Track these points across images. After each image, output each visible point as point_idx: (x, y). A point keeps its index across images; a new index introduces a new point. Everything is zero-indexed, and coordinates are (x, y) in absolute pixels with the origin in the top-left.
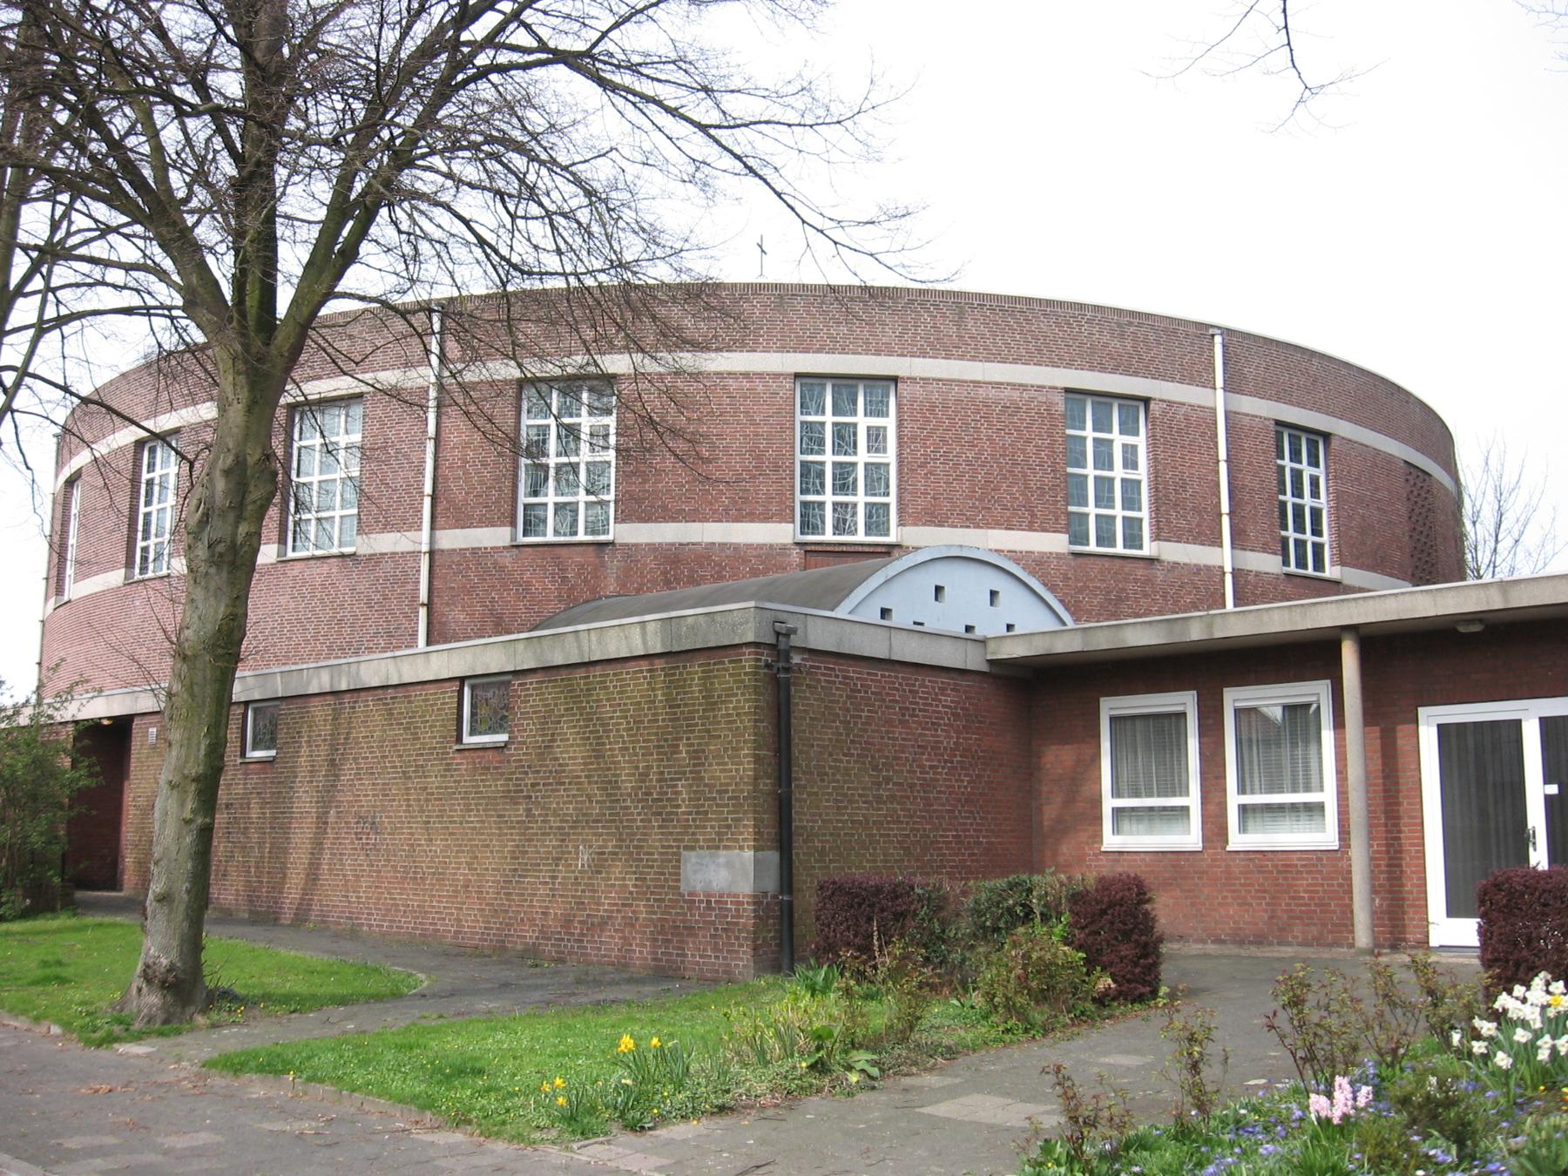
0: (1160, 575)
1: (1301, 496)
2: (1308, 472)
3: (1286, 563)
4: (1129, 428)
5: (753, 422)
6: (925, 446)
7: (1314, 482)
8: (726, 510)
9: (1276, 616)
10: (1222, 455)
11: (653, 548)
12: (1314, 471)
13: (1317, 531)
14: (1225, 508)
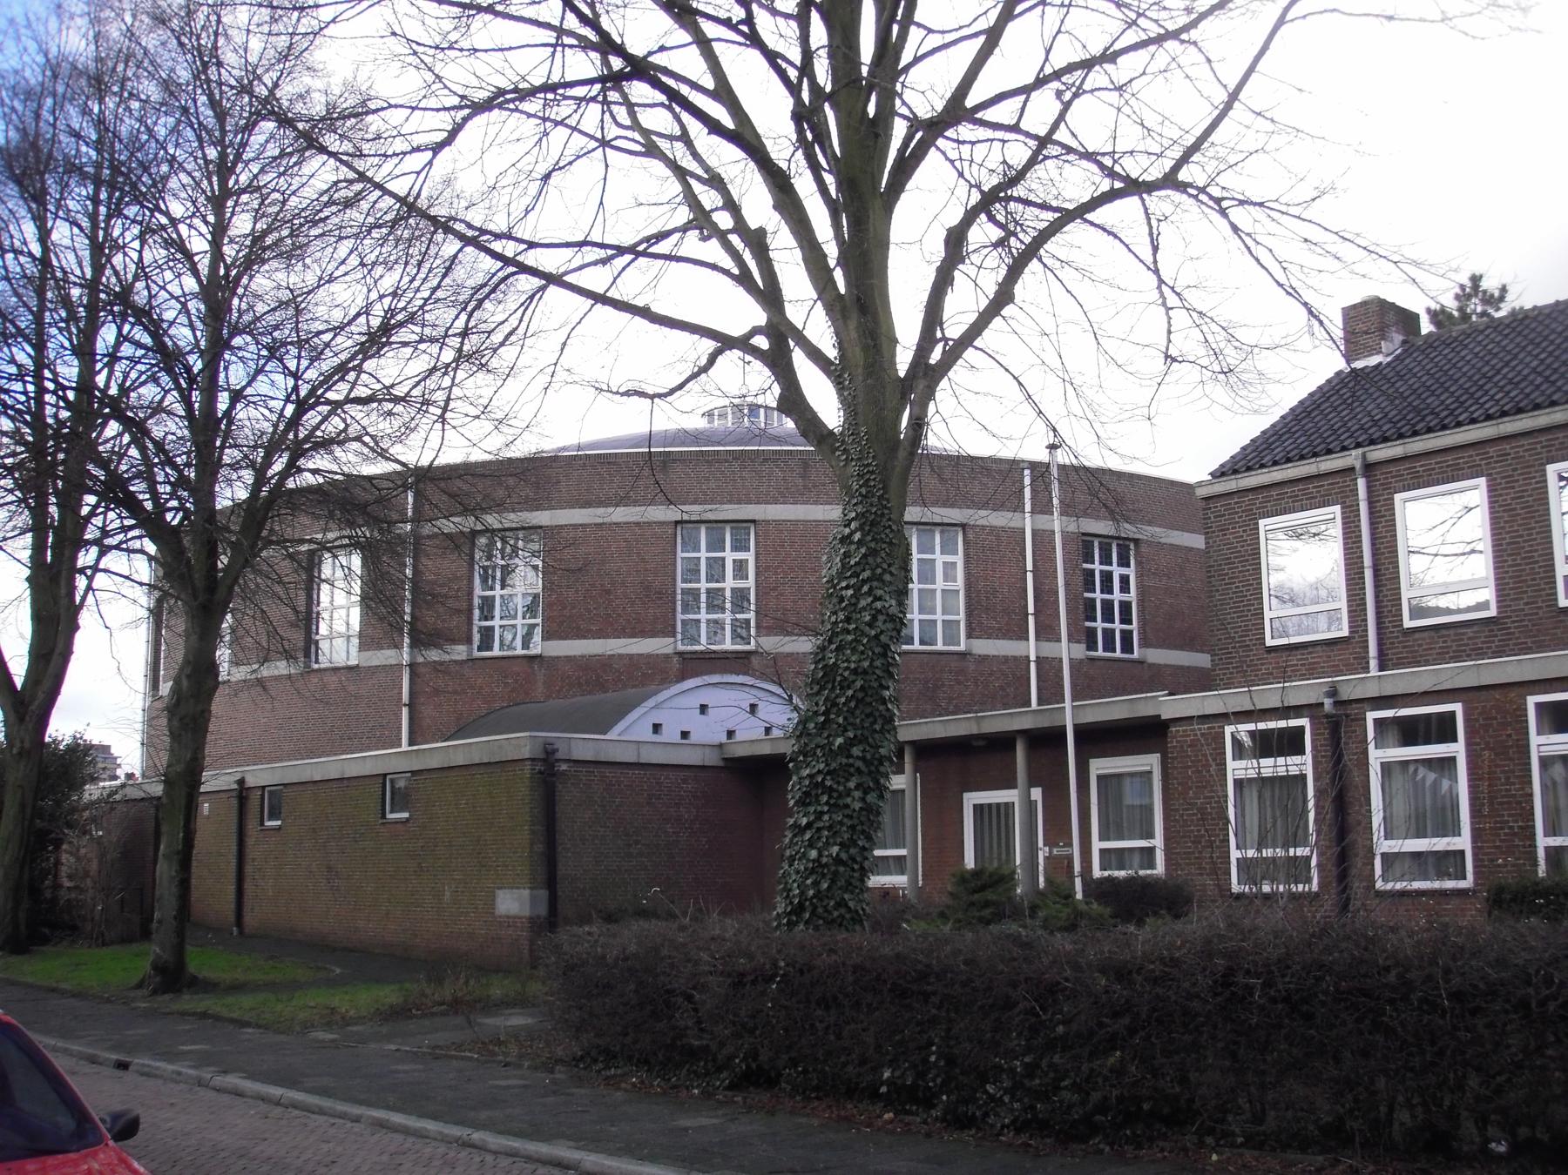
0: (972, 667)
2: (1117, 571)
4: (948, 548)
5: (643, 560)
6: (776, 574)
7: (1125, 580)
8: (624, 629)
9: (924, 728)
10: (1029, 566)
11: (569, 659)
12: (1124, 571)
14: (1031, 609)
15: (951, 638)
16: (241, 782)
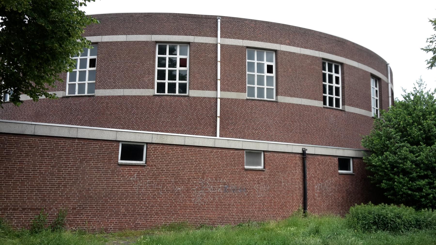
1: (332, 83)
2: (334, 75)
3: (325, 103)
7: (337, 78)
12: (337, 75)
13: (337, 94)
15: (270, 95)
16: (304, 151)
